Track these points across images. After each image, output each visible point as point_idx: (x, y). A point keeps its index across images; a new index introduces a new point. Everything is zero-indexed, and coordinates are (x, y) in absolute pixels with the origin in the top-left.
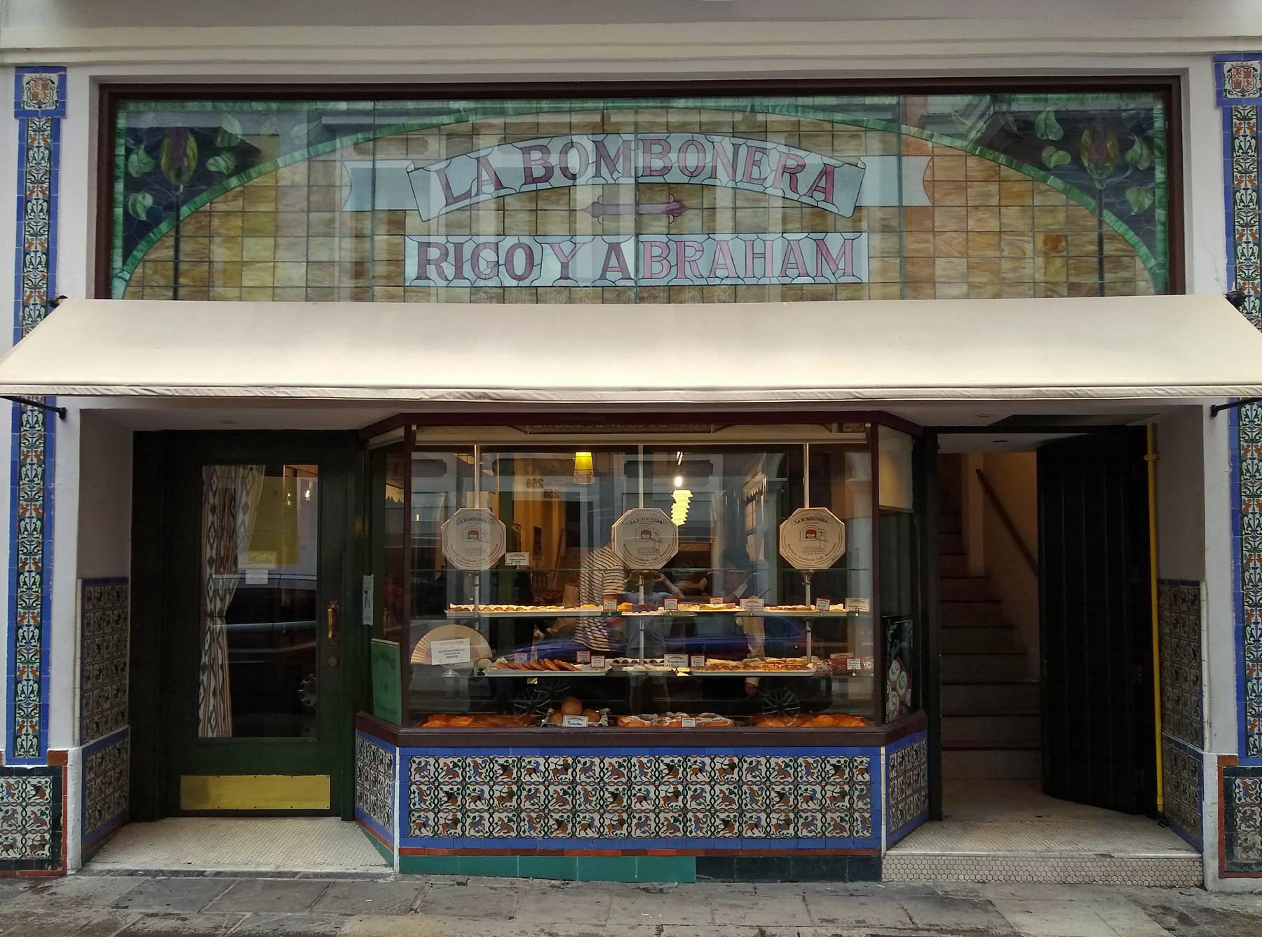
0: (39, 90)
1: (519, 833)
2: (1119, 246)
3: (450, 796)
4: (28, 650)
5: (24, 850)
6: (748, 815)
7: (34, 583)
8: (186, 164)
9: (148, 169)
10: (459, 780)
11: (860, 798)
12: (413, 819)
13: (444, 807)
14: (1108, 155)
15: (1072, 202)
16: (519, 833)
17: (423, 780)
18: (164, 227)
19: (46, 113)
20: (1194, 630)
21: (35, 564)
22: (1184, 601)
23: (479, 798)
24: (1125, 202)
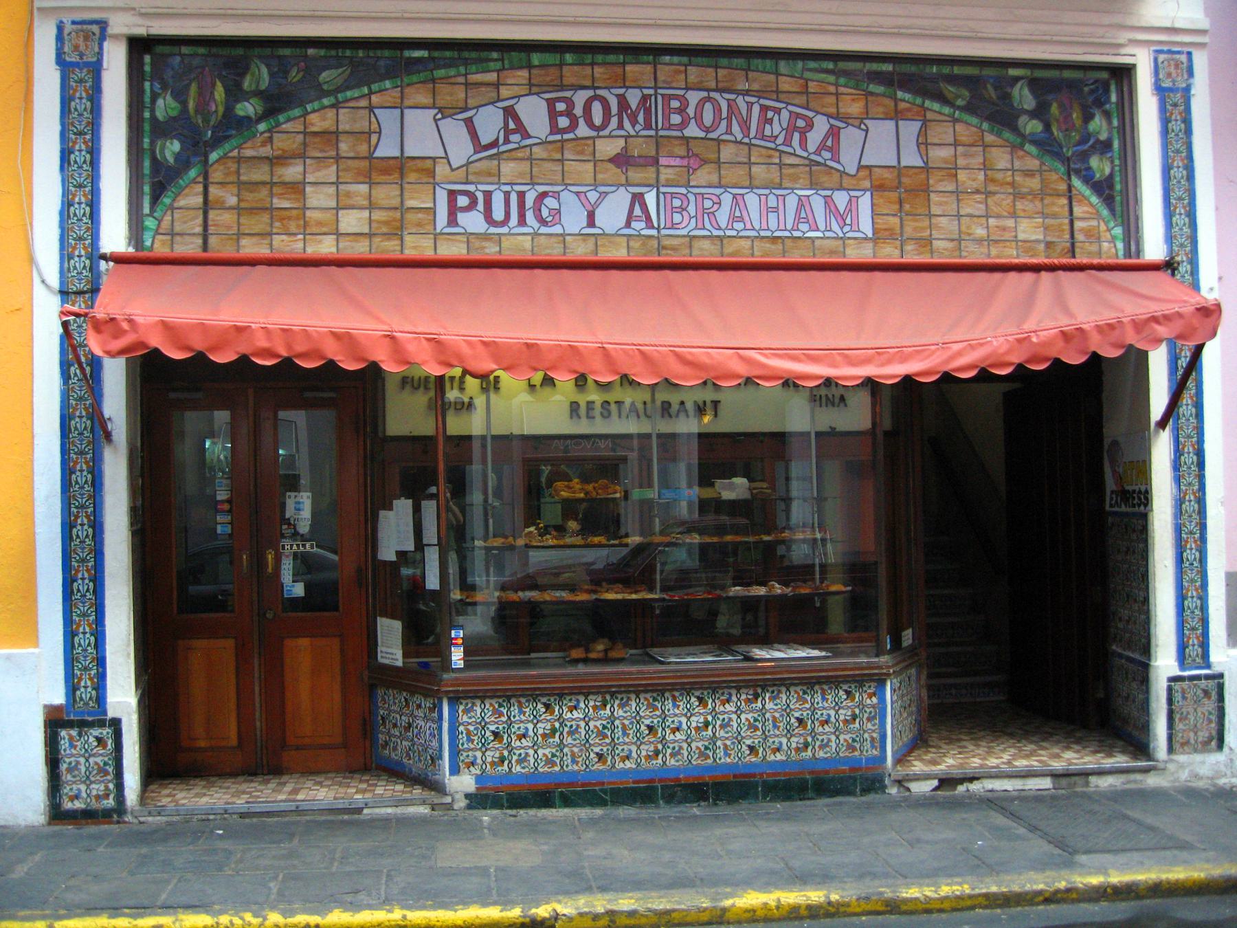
0: (81, 42)
1: (562, 767)
2: (1086, 209)
3: (496, 735)
4: (84, 603)
5: (89, 800)
6: (771, 740)
7: (87, 536)
8: (214, 109)
9: (174, 113)
10: (504, 719)
11: (869, 719)
12: (462, 758)
13: (491, 745)
14: (1074, 125)
15: (1046, 168)
16: (562, 767)
17: (470, 721)
18: (193, 173)
19: (87, 64)
20: (1143, 557)
21: (87, 517)
22: (1134, 531)
23: (524, 736)
24: (1089, 168)
